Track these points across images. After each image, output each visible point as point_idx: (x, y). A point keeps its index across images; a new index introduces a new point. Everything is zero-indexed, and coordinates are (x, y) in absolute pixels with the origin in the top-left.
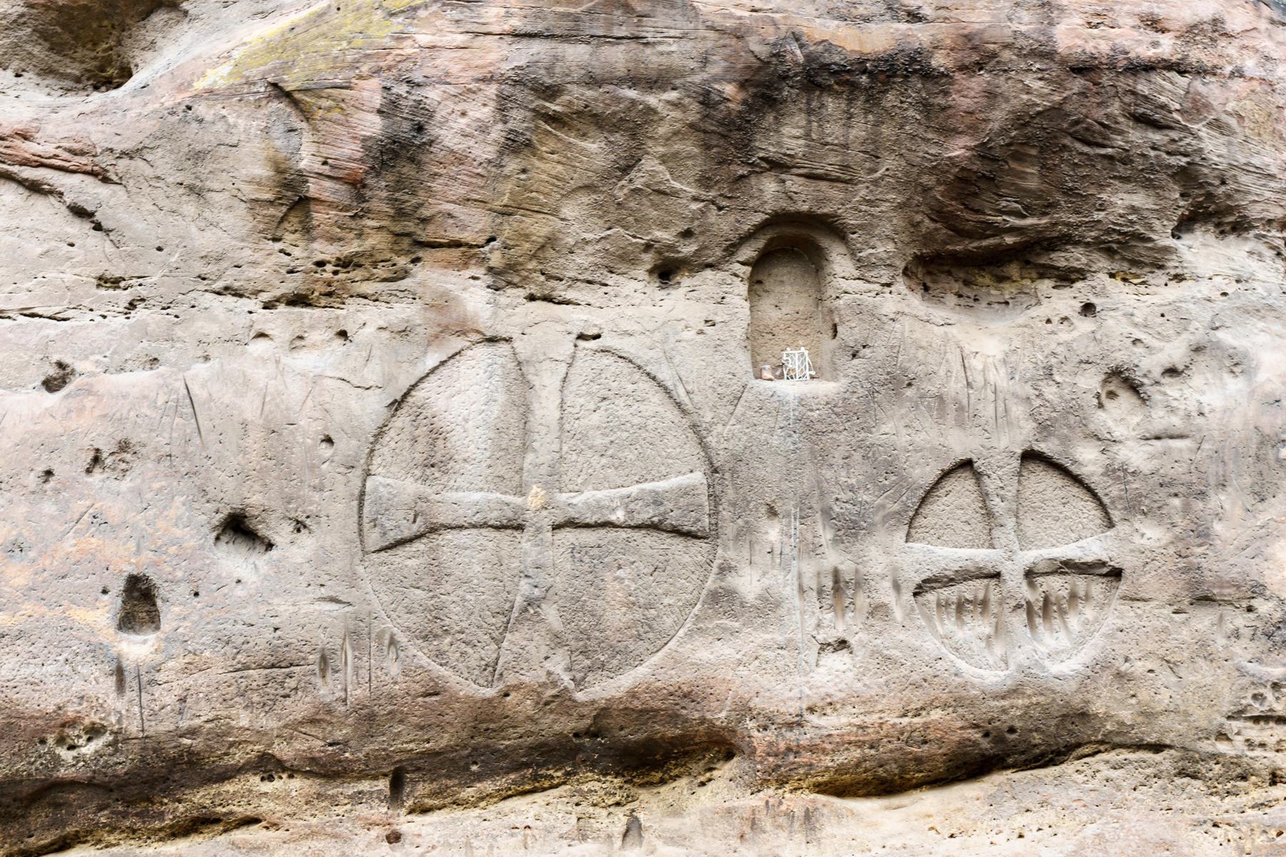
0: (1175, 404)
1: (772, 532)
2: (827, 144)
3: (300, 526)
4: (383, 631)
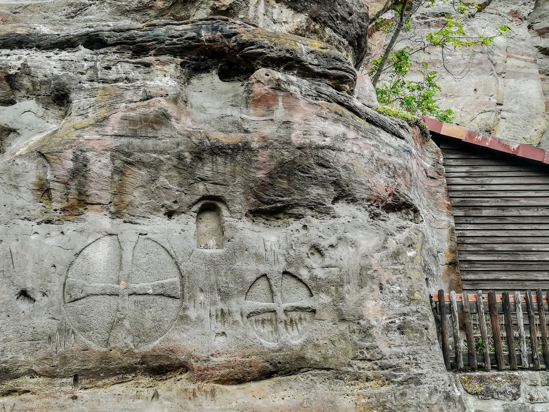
0: (332, 256)
1: (201, 297)
2: (219, 173)
3: (44, 294)
4: (69, 329)
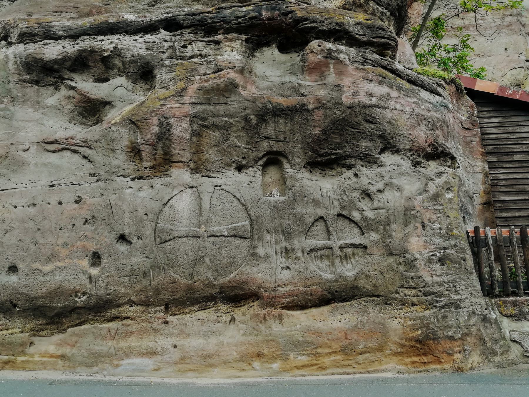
0: (380, 200)
2: (280, 131)
3: (139, 238)
